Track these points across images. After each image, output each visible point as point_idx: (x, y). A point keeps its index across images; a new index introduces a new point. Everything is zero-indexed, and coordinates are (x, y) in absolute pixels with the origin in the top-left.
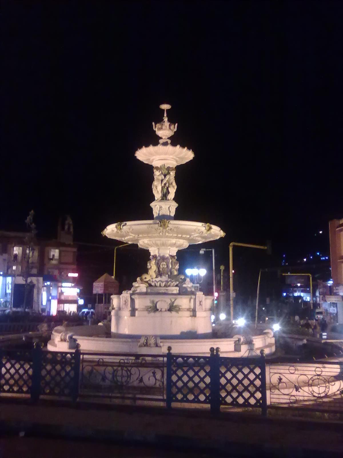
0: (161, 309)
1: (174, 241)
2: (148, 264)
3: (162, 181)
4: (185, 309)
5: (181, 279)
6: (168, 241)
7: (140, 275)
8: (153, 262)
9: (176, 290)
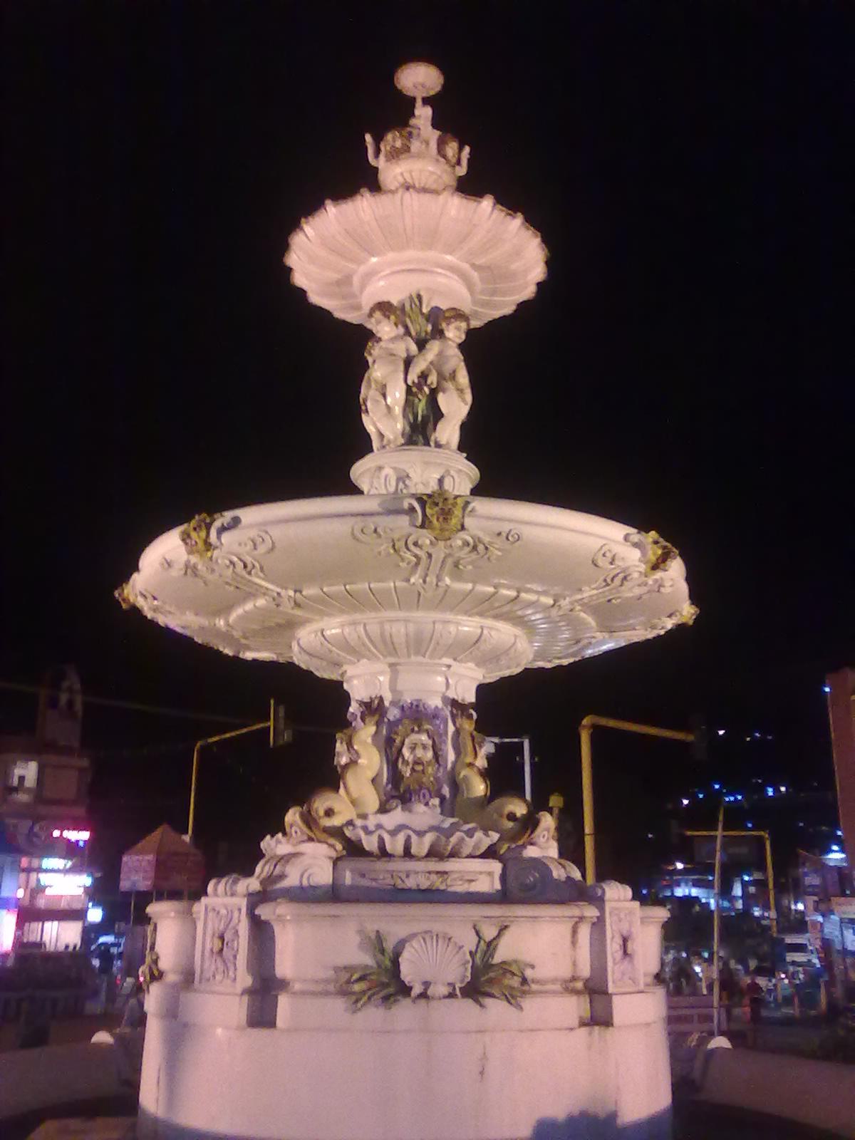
0: (427, 984)
1: (468, 626)
2: (340, 747)
3: (408, 363)
4: (554, 981)
5: (511, 817)
6: (448, 622)
7: (302, 798)
8: (365, 733)
9: (486, 876)
